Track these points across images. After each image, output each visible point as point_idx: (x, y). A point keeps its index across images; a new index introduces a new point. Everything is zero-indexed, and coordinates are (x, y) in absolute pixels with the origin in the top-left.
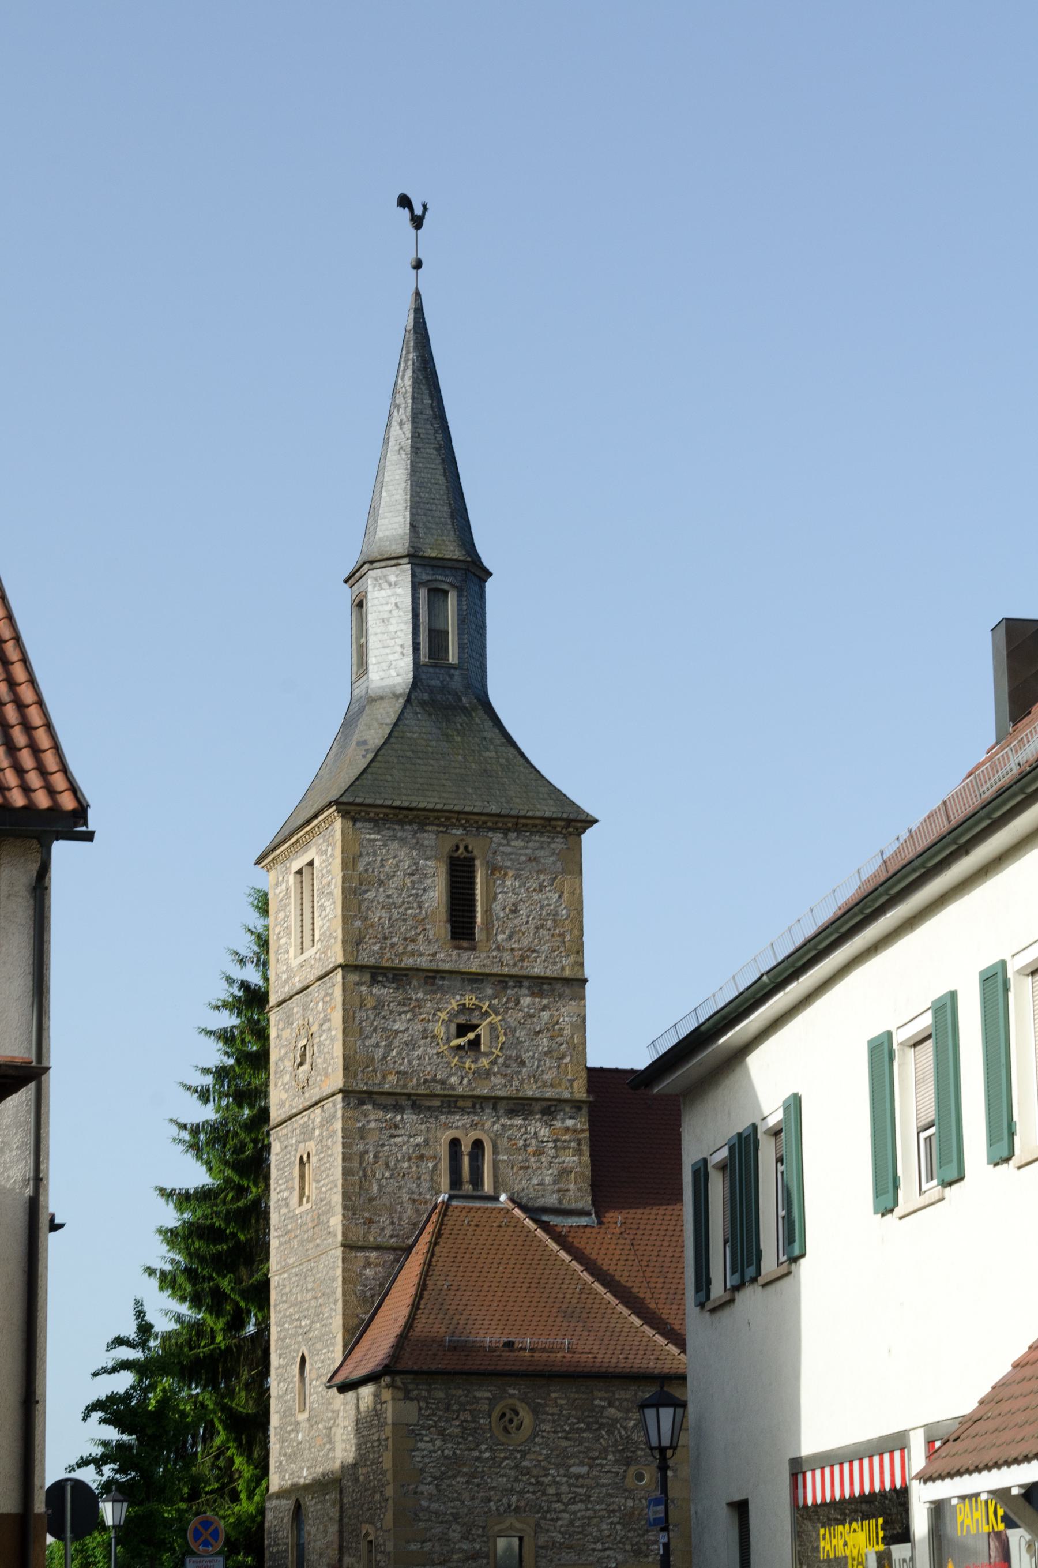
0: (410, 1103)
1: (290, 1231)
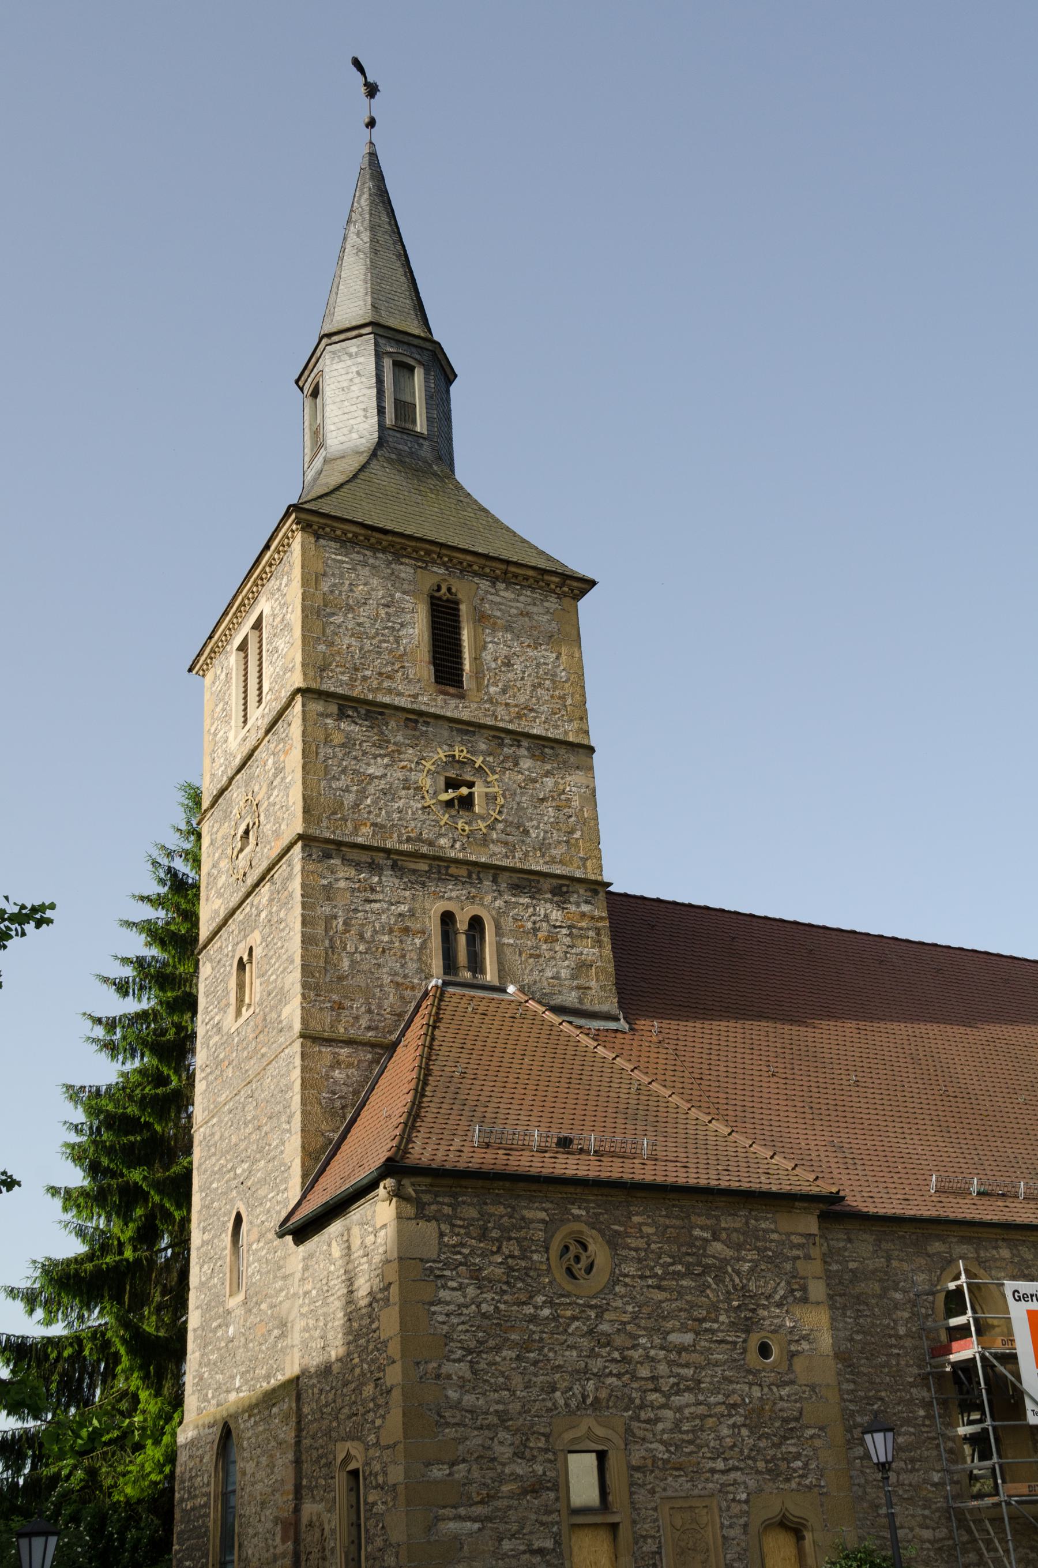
0: (390, 863)
1: (223, 1061)
